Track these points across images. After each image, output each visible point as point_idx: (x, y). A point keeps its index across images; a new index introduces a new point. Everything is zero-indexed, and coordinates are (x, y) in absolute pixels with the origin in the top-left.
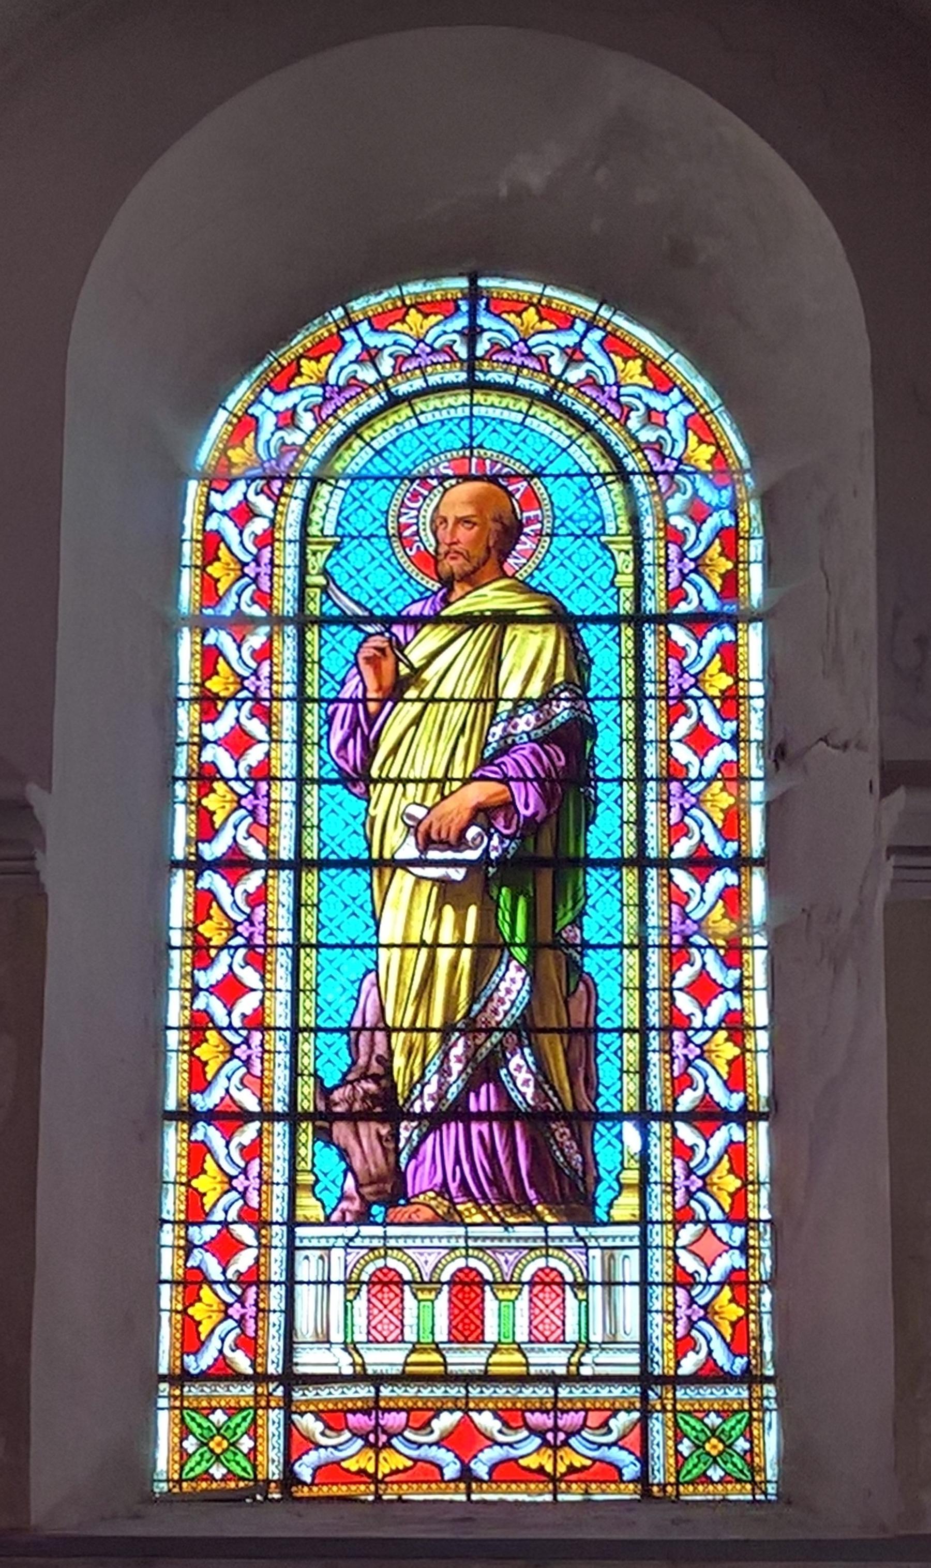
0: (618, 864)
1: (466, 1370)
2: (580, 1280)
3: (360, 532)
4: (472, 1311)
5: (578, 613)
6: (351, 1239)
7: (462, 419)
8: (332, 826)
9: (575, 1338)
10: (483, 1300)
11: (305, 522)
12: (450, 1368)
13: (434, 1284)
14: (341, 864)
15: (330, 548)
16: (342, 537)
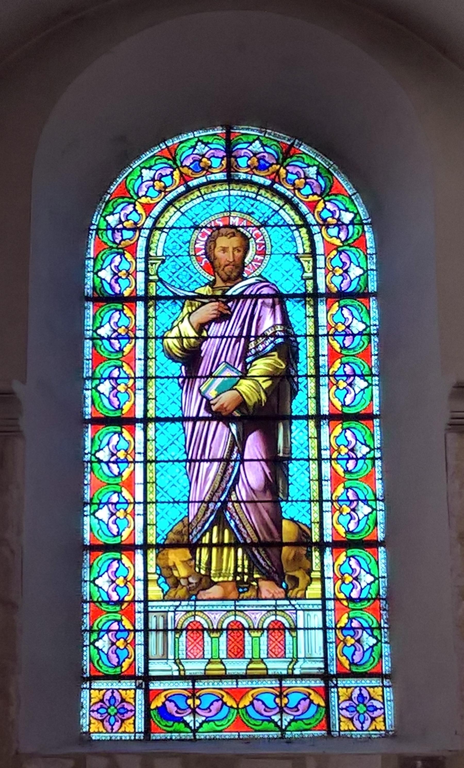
0: (307, 417)
1: (236, 672)
2: (293, 627)
3: (174, 254)
4: (198, 643)
5: (285, 293)
6: (177, 607)
7: (225, 196)
8: (162, 399)
9: (291, 656)
10: (244, 637)
11: (148, 249)
12: (228, 672)
13: (220, 630)
14: (167, 420)
15: (160, 262)
16: (166, 256)
